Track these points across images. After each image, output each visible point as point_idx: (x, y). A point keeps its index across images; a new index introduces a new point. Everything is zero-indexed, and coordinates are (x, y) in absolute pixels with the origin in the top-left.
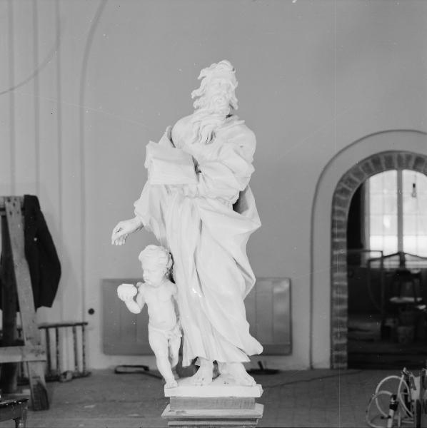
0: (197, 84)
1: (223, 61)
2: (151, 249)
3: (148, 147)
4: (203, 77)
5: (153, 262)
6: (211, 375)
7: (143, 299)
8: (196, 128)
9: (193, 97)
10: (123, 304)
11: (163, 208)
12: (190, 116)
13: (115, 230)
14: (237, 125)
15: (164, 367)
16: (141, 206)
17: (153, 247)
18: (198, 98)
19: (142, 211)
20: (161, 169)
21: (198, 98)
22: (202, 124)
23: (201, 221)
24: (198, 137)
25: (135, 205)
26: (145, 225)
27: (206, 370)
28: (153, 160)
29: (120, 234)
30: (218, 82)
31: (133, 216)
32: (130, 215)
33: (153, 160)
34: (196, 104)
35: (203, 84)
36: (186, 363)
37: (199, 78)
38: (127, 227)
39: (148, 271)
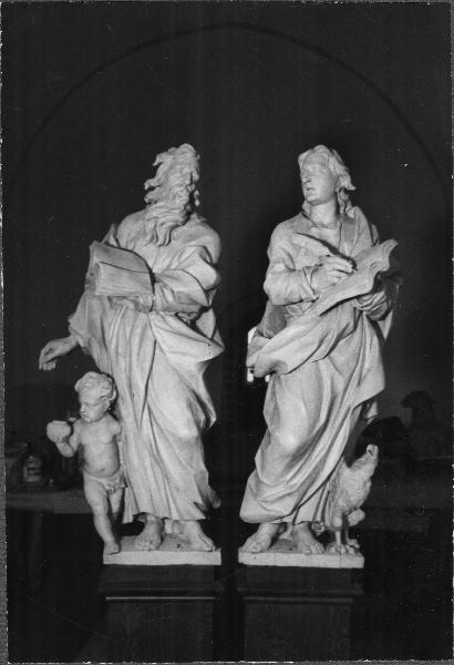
0: (152, 173)
1: (186, 145)
2: (91, 377)
3: (91, 248)
4: (160, 164)
5: (91, 391)
6: (156, 539)
7: (79, 438)
8: (151, 225)
9: (372, 449)
10: (52, 445)
11: (106, 325)
12: (143, 212)
13: (43, 351)
14: (195, 225)
15: (103, 526)
16: (77, 322)
17: (94, 374)
18: (152, 189)
19: (80, 327)
20: (105, 277)
21: (152, 189)
22: (161, 221)
23: (322, 315)
24: (155, 238)
25: (70, 321)
26: (82, 345)
27: (150, 531)
28: (101, 265)
29: (50, 356)
30: (177, 169)
31: (67, 334)
32: (64, 332)
33: (101, 265)
34: (150, 196)
35: (160, 171)
36: (128, 518)
37: (155, 164)
38: (60, 347)
39: (87, 404)
